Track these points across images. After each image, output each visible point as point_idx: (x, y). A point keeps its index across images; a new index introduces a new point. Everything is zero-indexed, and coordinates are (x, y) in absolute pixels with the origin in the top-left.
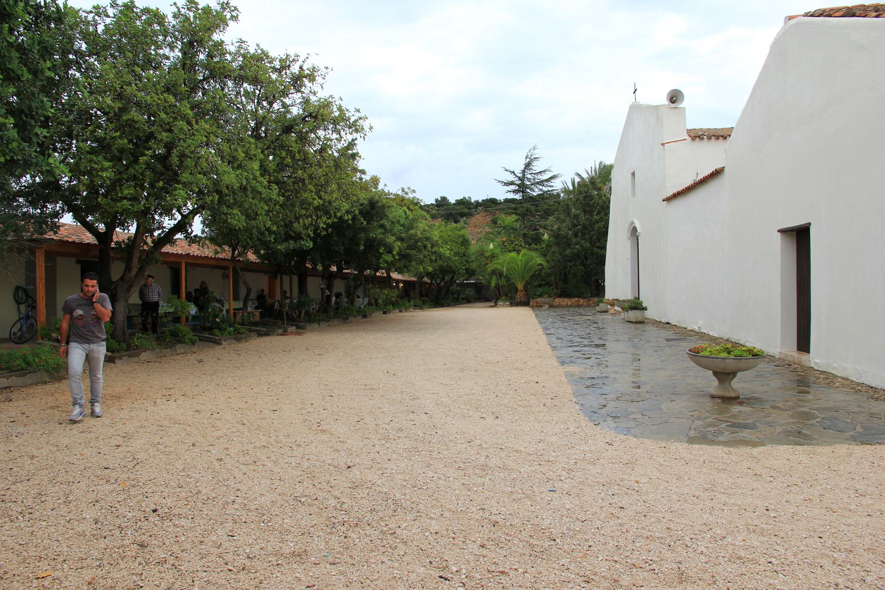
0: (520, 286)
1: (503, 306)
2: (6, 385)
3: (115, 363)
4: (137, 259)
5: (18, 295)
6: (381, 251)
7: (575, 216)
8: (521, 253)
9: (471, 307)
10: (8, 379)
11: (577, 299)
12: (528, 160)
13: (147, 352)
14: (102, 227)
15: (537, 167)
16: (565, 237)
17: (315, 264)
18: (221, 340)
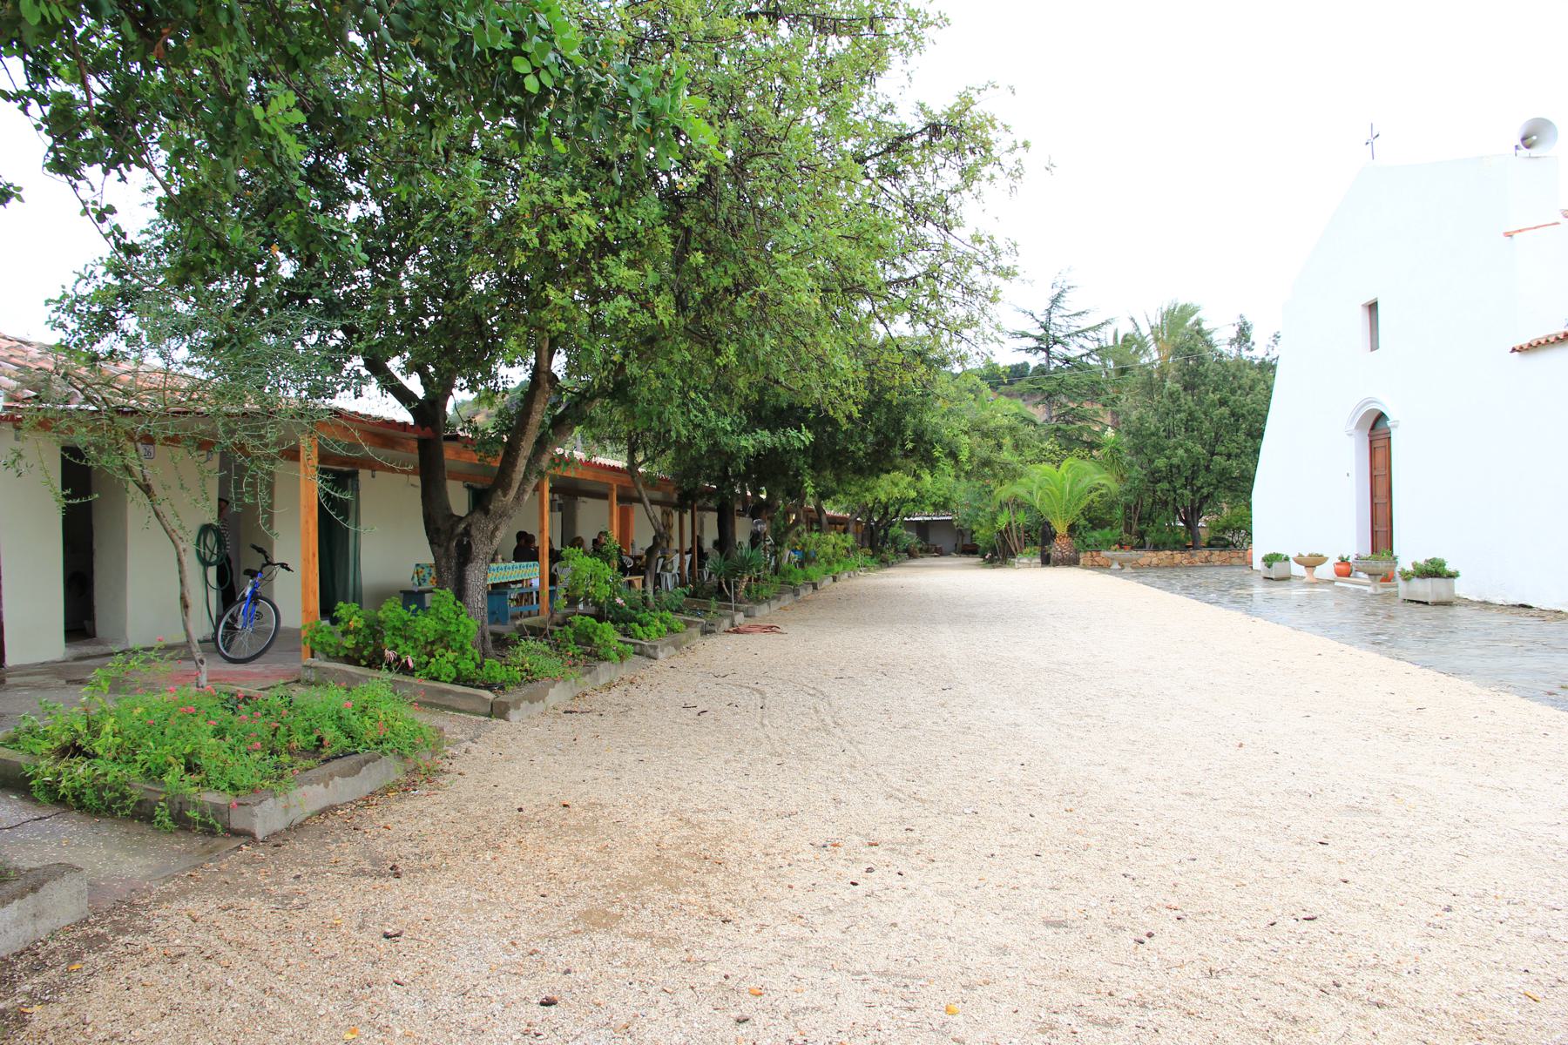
0: (1060, 527)
1: (1029, 566)
2: (323, 803)
3: (507, 720)
4: (525, 462)
5: (205, 544)
6: (937, 454)
7: (1171, 395)
8: (1064, 465)
9: (1139, 570)
10: (326, 786)
11: (1169, 552)
12: (1056, 291)
13: (557, 685)
14: (414, 384)
15: (1071, 303)
16: (1153, 434)
17: (743, 488)
18: (655, 648)
